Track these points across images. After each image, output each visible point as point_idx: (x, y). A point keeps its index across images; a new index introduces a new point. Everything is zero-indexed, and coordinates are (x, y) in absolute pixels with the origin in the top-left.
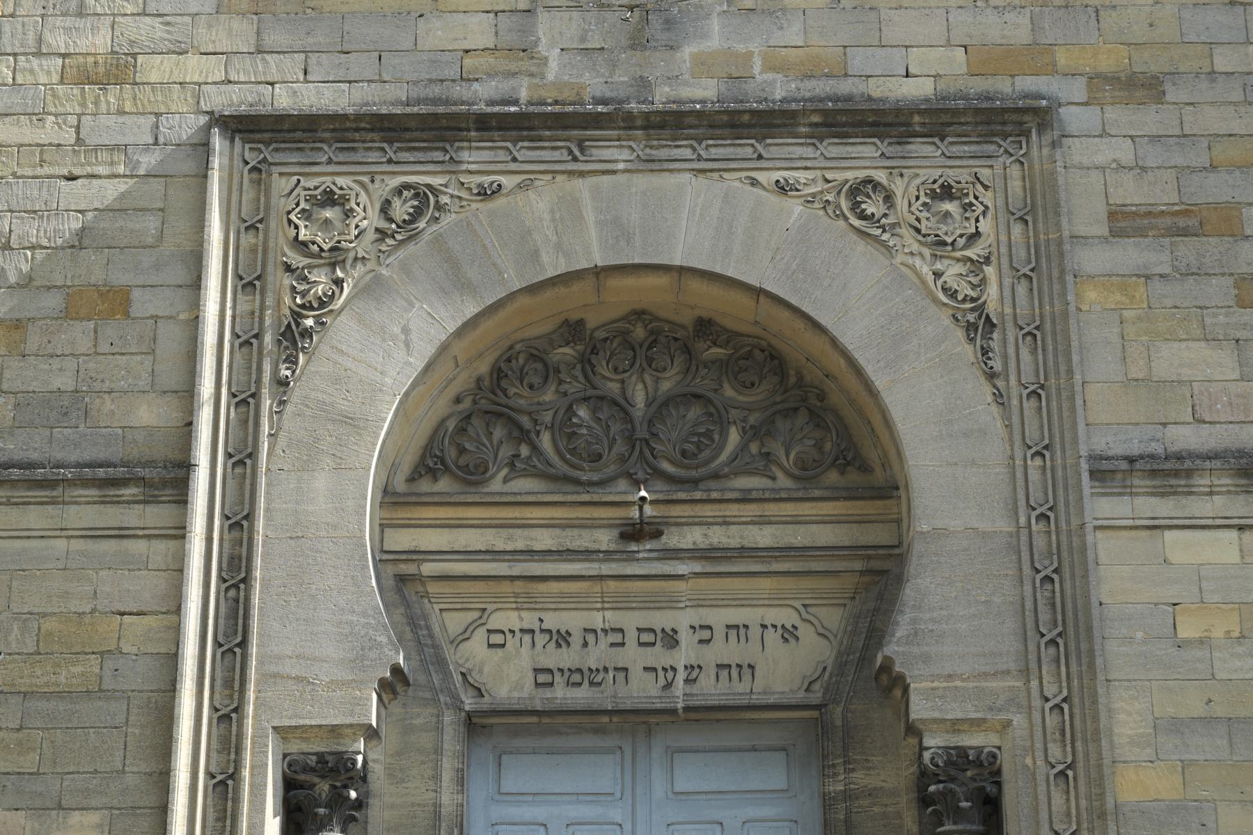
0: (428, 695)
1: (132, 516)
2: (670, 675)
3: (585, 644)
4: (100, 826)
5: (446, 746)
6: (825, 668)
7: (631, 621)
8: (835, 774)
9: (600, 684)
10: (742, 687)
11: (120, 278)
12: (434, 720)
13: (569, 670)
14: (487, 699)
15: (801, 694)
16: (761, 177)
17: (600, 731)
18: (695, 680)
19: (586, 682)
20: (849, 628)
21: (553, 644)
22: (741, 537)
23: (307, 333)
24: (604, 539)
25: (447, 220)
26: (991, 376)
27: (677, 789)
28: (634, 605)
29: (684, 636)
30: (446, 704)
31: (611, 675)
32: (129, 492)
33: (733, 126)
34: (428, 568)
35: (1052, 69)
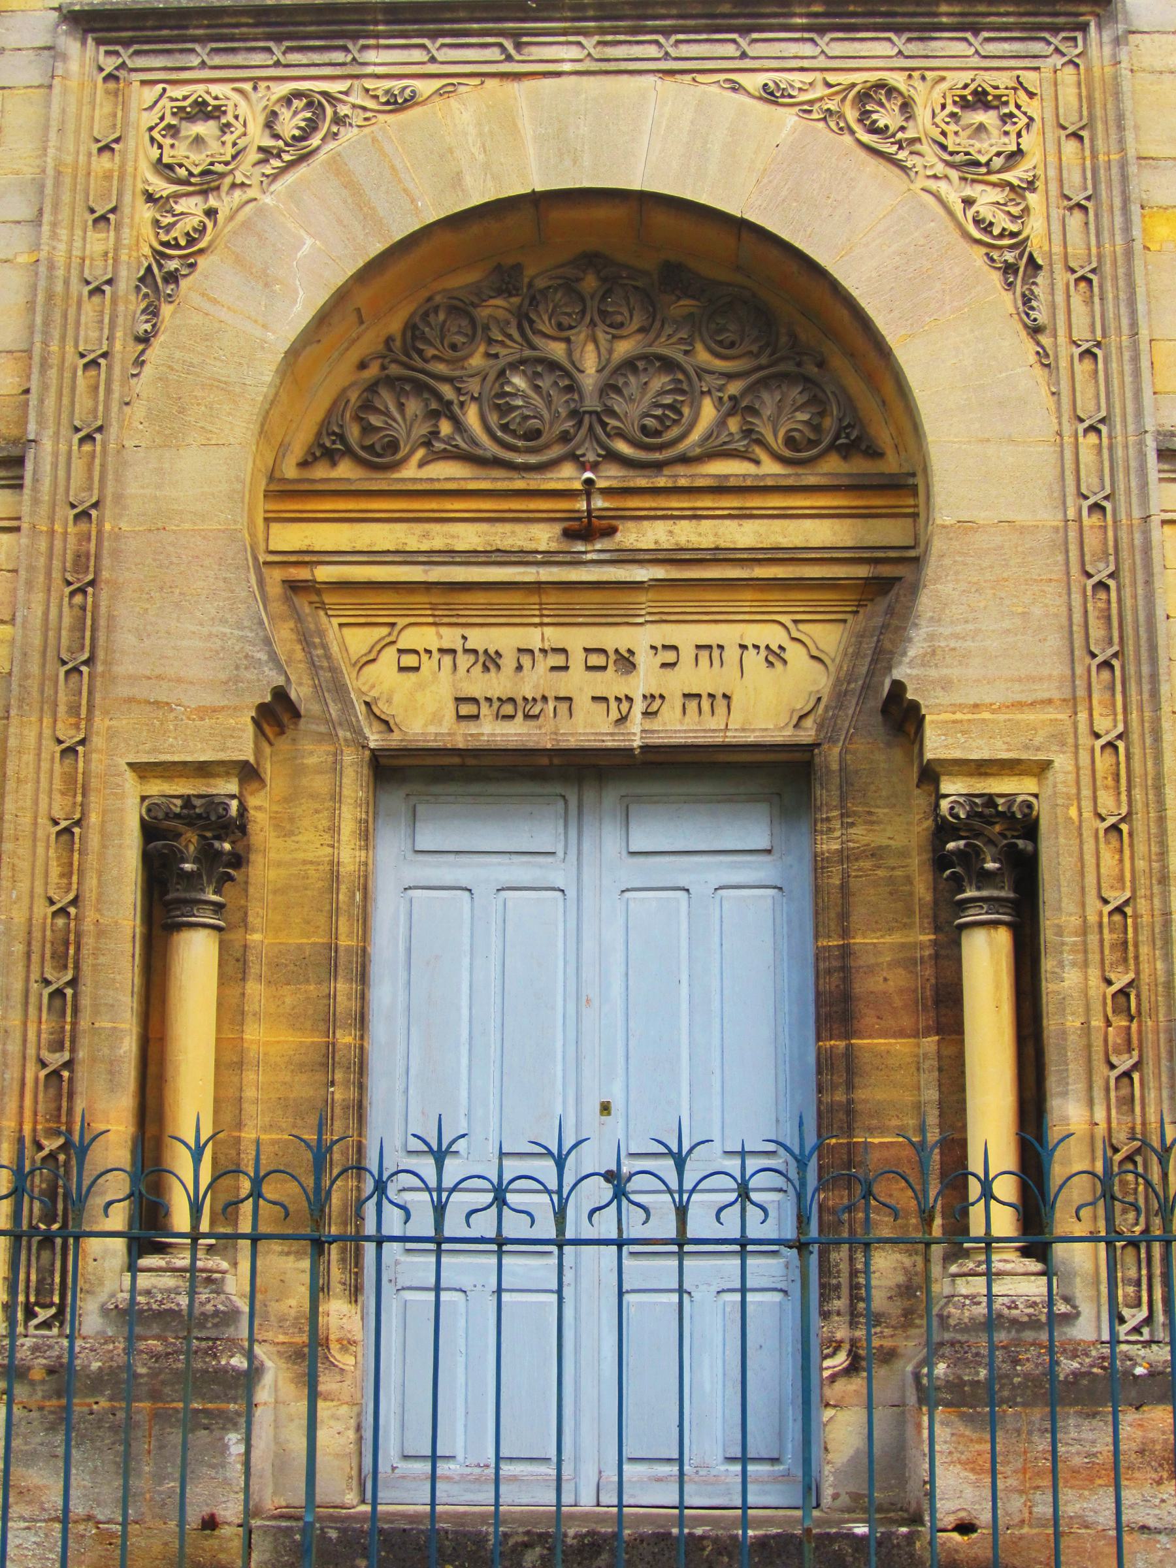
0: (323, 729)
2: (625, 706)
3: (520, 668)
5: (345, 792)
6: (819, 699)
7: (577, 639)
8: (830, 830)
9: (537, 717)
12: (330, 759)
13: (499, 699)
15: (789, 732)
18: (656, 713)
19: (520, 714)
20: (850, 650)
21: (479, 666)
22: (716, 535)
24: (544, 537)
25: (348, 135)
26: (1035, 330)
27: (633, 849)
28: (581, 620)
29: (644, 659)
30: (346, 740)
31: (551, 704)
34: (324, 573)
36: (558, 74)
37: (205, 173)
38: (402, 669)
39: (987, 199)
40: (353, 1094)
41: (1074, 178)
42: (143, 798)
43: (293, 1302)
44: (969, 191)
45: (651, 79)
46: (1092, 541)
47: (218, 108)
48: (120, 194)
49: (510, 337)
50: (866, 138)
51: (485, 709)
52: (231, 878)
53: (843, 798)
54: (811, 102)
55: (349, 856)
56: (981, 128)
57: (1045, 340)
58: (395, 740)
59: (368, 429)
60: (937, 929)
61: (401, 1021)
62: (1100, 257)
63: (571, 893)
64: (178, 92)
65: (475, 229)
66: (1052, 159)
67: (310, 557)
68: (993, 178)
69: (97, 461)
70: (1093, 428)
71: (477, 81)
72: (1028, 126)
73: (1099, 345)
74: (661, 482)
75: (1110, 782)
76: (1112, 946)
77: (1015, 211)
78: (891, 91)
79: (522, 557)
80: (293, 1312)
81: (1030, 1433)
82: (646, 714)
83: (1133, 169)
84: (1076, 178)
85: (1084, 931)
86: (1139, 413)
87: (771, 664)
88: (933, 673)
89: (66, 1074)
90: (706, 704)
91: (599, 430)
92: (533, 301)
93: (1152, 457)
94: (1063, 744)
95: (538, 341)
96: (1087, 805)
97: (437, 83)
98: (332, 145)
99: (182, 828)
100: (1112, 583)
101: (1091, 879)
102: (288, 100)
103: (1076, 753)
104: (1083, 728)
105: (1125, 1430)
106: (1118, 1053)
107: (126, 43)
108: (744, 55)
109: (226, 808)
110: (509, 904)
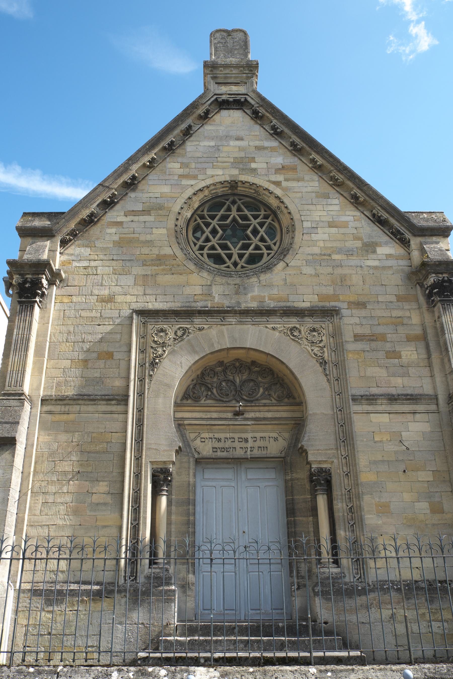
0: (186, 454)
1: (114, 408)
2: (246, 449)
3: (225, 442)
4: (107, 485)
7: (236, 436)
8: (288, 474)
10: (264, 452)
11: (111, 350)
14: (201, 455)
15: (279, 454)
16: (268, 326)
17: (228, 463)
21: (217, 441)
23: (157, 363)
24: (230, 415)
25: (191, 336)
26: (326, 375)
27: (248, 478)
29: (250, 440)
32: (113, 402)
33: (261, 313)
34: (186, 422)
35: (339, 300)
36: (232, 324)
37: (163, 343)
38: (201, 442)
39: (316, 349)
40: (193, 530)
41: (332, 345)
42: (152, 468)
43: (182, 575)
44: (313, 348)
45: (250, 325)
46: (339, 416)
47: (165, 330)
48: (146, 347)
49: (222, 375)
50: (292, 337)
51: (218, 450)
52: (169, 484)
53: (291, 468)
54: (281, 330)
55: (192, 480)
56: (314, 335)
57: (328, 377)
58: (200, 456)
59: (194, 393)
60: (311, 495)
61: (201, 514)
62: (338, 360)
63: (236, 487)
64: (157, 327)
65: (216, 354)
66: (328, 341)
67: (183, 419)
68: (317, 345)
69: (142, 400)
70: (338, 394)
71: (216, 326)
72: (323, 335)
73: (339, 378)
74: (253, 404)
75: (345, 465)
76: (348, 498)
77: (322, 352)
78: (297, 328)
79: (225, 419)
80: (182, 577)
81: (338, 602)
82: (250, 451)
83: (344, 344)
84: (333, 345)
85: (342, 495)
86: (348, 391)
87: (275, 441)
88: (310, 443)
89: (137, 526)
90: (262, 449)
91: (240, 394)
92: (226, 369)
93: (351, 400)
94: (336, 457)
95: (227, 376)
96: (341, 469)
97: (208, 326)
98: (188, 338)
99: (160, 475)
100: (344, 425)
101: (343, 485)
102: (179, 329)
103: (338, 459)
104: (340, 454)
105: (358, 601)
106: (350, 520)
107: (147, 317)
108: (268, 321)
109: (170, 470)
110: (223, 489)
